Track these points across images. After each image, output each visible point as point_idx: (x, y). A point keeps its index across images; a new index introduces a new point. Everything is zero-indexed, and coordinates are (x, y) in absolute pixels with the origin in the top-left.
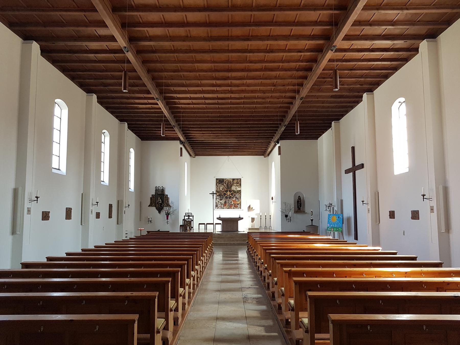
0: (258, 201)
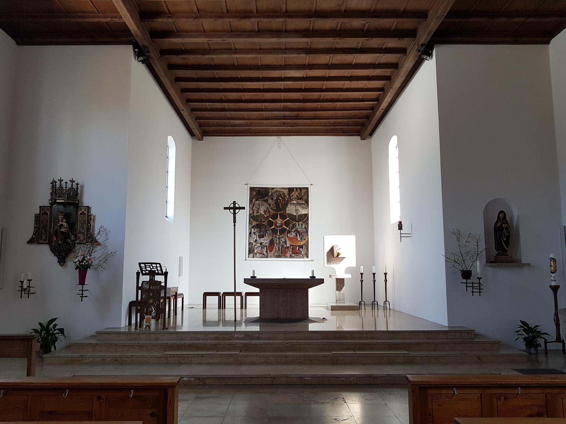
0: (352, 239)
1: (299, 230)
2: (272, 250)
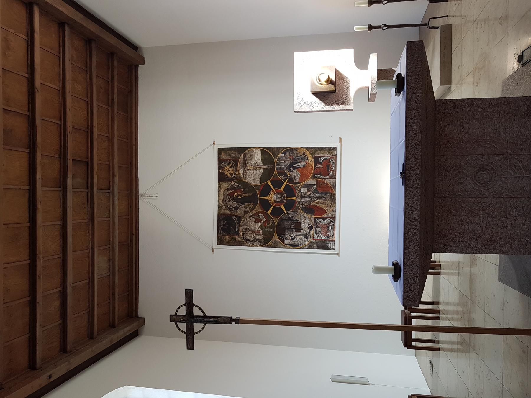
1: (288, 163)
2: (322, 209)
